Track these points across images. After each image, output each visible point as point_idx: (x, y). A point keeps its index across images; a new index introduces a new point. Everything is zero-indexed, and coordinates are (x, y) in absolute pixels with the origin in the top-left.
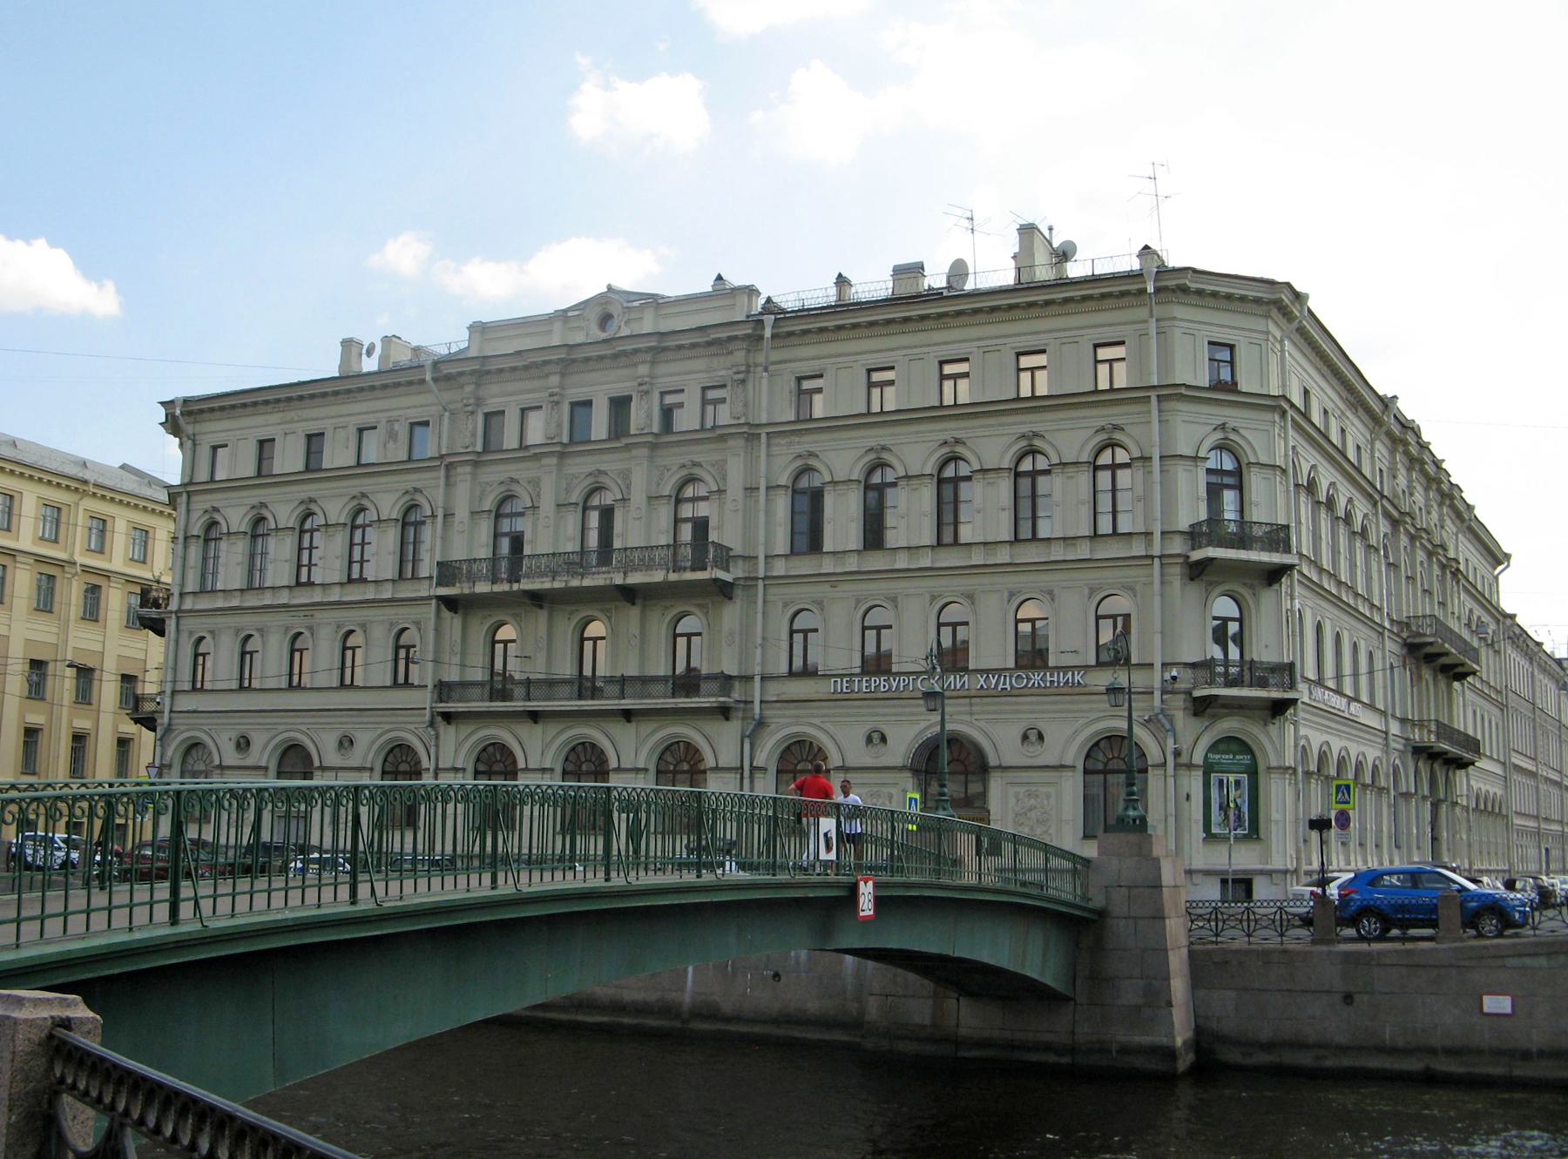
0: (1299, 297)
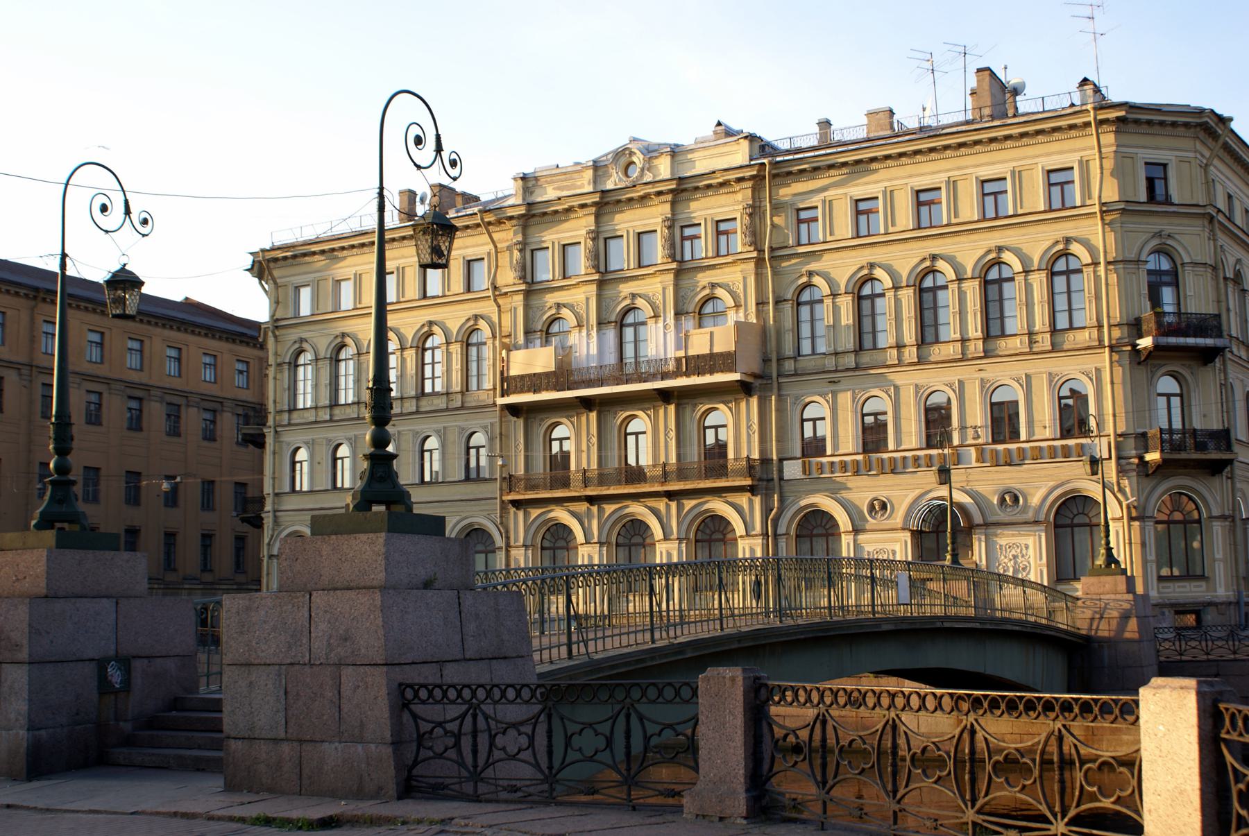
0: (1224, 121)
